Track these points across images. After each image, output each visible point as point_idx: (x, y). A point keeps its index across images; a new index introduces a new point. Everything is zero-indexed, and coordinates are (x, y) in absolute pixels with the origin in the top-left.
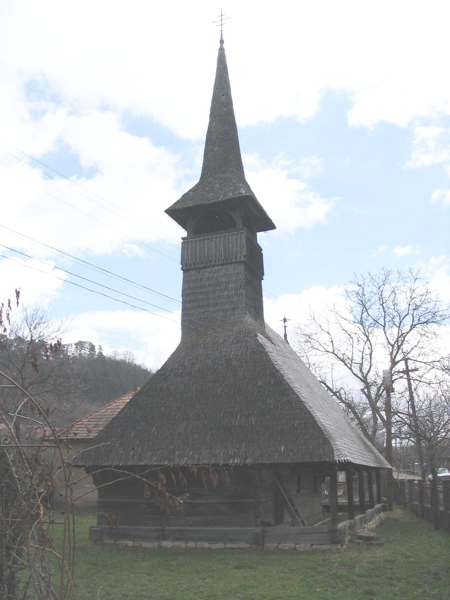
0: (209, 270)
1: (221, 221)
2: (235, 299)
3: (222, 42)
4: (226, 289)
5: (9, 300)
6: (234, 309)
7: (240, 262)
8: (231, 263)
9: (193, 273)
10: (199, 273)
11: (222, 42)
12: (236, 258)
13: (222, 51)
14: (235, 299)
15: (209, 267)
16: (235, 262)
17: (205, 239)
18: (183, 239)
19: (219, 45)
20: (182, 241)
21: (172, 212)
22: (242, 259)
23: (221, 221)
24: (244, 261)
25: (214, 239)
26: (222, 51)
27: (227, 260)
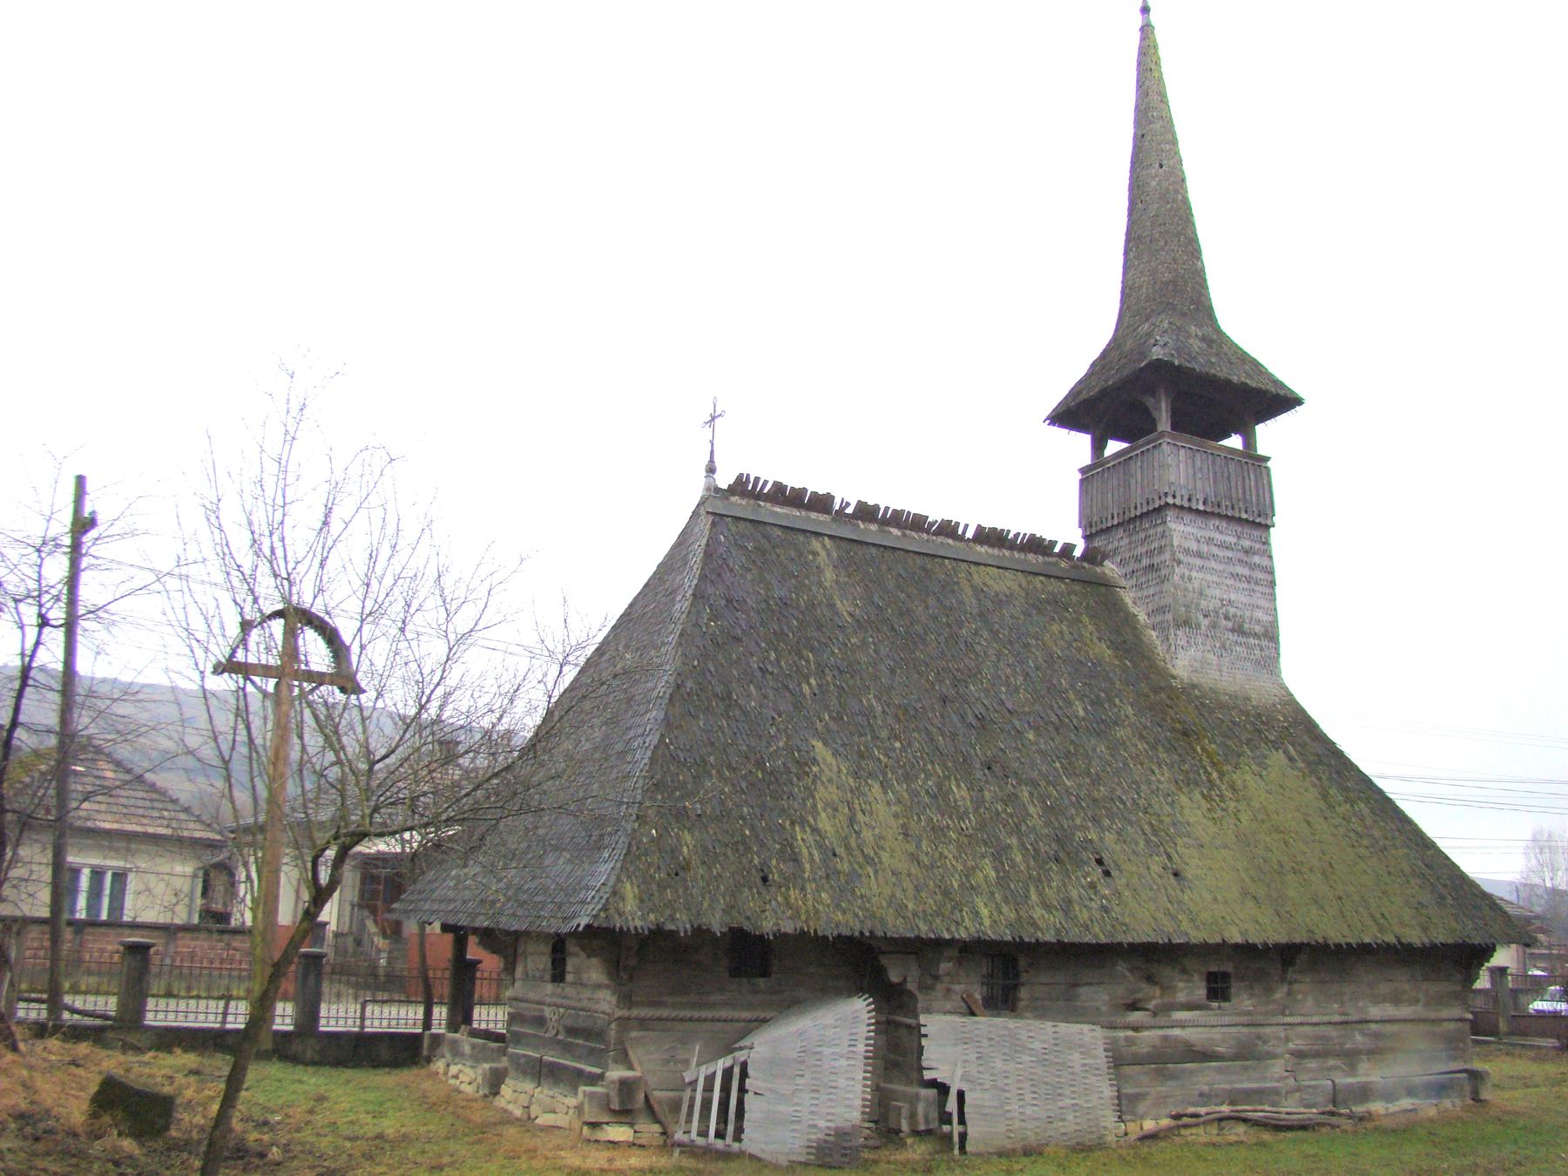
3: (1145, 10)
5: (81, 481)
11: (1145, 10)
13: (1146, 30)
19: (1138, 21)
21: (1068, 416)
23: (1174, 396)
26: (1146, 30)
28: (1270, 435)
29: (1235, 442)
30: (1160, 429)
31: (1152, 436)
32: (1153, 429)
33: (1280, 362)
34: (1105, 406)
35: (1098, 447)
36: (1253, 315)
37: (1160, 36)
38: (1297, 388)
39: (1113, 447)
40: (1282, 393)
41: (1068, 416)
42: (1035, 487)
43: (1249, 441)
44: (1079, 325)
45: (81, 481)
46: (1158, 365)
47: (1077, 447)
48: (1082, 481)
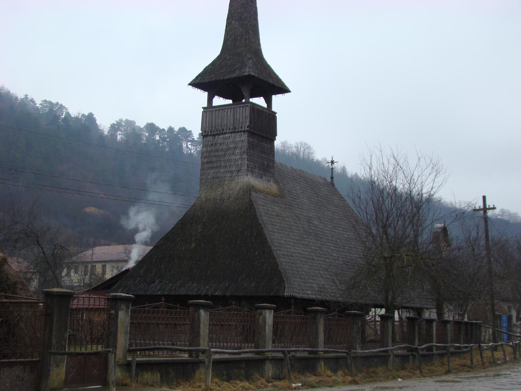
0: (222, 136)
1: (240, 77)
2: (240, 162)
4: (233, 154)
5: (484, 198)
6: (239, 171)
7: (244, 131)
8: (238, 132)
9: (210, 138)
10: (215, 138)
12: (241, 128)
14: (240, 162)
15: (222, 134)
16: (241, 132)
18: (204, 108)
20: (203, 110)
22: (246, 129)
24: (247, 131)
25: (226, 110)
27: (235, 129)
29: (260, 101)
35: (210, 100)
38: (290, 89)
39: (218, 101)
43: (269, 101)
44: (209, 48)
45: (484, 198)
47: (201, 97)
48: (203, 112)
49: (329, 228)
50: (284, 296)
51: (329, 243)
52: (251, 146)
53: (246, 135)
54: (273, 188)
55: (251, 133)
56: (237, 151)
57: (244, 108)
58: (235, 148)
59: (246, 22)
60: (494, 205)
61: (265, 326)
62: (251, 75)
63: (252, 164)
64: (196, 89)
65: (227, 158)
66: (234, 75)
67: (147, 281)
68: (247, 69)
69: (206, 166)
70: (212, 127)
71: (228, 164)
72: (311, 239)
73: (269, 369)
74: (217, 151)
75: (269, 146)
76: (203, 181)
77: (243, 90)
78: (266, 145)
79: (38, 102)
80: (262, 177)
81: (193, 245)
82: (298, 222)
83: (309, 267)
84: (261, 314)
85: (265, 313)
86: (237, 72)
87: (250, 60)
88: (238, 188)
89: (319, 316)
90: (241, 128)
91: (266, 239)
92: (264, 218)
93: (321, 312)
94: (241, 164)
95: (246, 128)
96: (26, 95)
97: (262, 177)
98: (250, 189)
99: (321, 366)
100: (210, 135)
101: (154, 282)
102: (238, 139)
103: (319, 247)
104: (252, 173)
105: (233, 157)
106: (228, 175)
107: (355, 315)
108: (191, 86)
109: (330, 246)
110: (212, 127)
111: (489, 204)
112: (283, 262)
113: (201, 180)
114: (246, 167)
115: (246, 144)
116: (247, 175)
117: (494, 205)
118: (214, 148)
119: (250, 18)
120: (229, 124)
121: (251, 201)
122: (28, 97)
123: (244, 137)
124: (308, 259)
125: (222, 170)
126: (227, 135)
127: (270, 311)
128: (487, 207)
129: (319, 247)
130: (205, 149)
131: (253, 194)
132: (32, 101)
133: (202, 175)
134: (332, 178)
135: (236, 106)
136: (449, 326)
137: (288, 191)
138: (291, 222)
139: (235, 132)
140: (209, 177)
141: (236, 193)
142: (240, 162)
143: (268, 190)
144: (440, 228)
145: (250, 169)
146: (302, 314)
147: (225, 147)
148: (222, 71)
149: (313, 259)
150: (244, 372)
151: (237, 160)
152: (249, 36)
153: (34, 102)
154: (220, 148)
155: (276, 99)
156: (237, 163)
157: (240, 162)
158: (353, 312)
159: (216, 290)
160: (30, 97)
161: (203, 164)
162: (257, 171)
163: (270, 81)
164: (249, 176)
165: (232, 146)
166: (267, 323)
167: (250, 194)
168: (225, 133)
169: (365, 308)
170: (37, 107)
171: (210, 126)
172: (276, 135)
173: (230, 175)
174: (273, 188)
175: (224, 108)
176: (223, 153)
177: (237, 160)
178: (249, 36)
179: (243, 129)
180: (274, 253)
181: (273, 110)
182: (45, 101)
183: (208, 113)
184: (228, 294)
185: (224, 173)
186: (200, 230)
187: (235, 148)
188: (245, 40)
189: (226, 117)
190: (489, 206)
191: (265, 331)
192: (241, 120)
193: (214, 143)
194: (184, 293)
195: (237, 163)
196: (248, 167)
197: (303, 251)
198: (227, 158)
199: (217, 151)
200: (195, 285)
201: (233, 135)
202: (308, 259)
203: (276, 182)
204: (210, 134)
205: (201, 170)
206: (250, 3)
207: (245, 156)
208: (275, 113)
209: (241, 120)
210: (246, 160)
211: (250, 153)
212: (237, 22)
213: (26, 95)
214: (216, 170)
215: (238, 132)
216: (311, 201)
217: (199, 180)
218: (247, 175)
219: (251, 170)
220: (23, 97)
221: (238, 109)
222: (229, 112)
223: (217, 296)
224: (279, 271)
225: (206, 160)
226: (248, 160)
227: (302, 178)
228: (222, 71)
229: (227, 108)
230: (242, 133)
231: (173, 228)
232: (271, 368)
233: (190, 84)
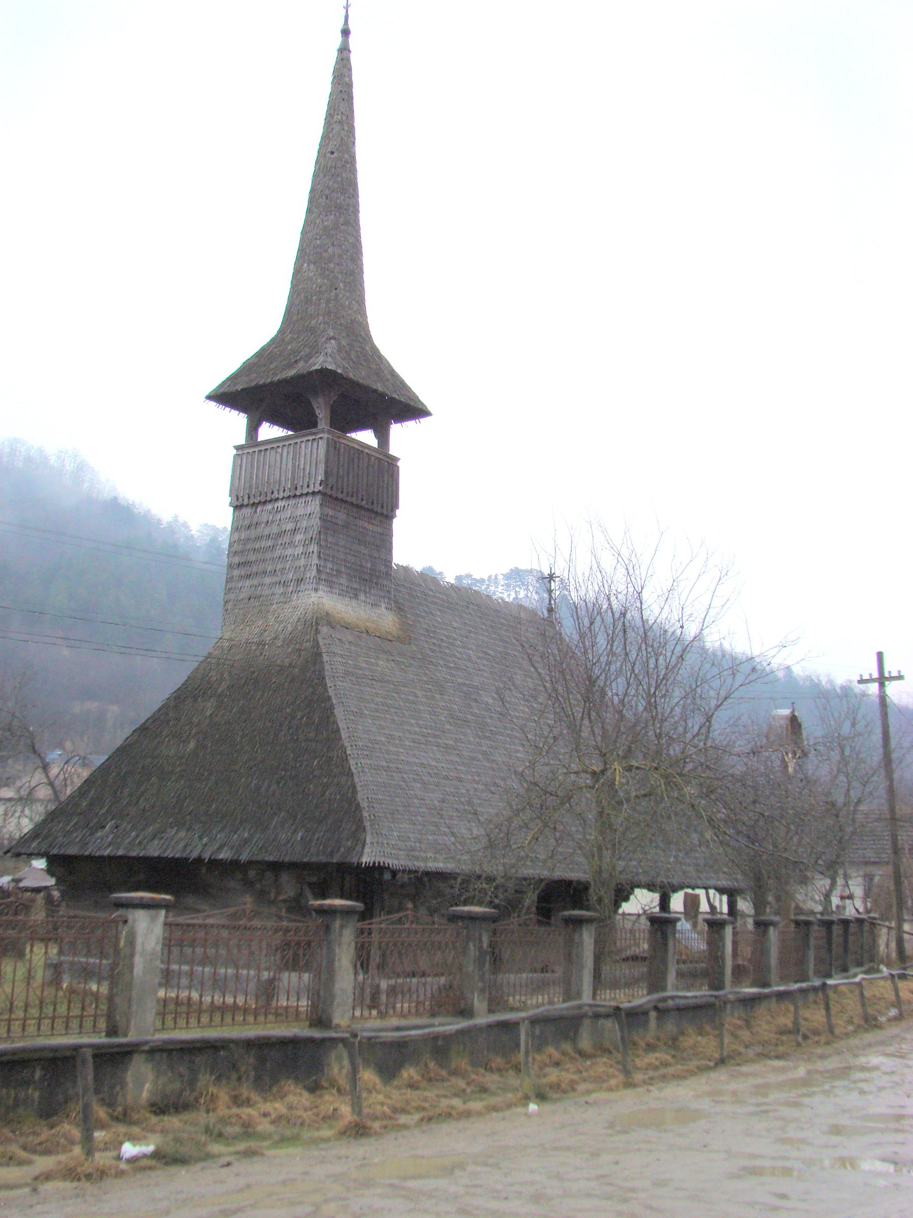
0: (269, 507)
1: (321, 395)
2: (302, 562)
3: (346, 33)
4: (291, 544)
5: (880, 656)
6: (300, 581)
7: (314, 493)
8: (301, 495)
9: (247, 511)
10: (256, 512)
11: (346, 33)
12: (308, 486)
13: (344, 51)
14: (302, 562)
15: (270, 501)
16: (307, 494)
17: (266, 450)
18: (238, 448)
19: (338, 39)
20: (235, 452)
21: (225, 397)
22: (318, 488)
23: (321, 395)
24: (319, 492)
25: (280, 450)
26: (344, 51)
27: (296, 488)
28: (403, 437)
29: (367, 437)
30: (320, 427)
31: (314, 430)
32: (315, 425)
33: (417, 378)
34: (261, 393)
35: (253, 430)
36: (400, 331)
37: (355, 60)
38: (430, 408)
39: (268, 432)
40: (359, 375)
41: (225, 397)
42: (546, 614)
43: (383, 436)
44: (251, 319)
45: (880, 656)
46: (325, 374)
47: (235, 423)
48: (236, 456)
49: (523, 712)
50: (359, 864)
51: (514, 744)
52: (327, 524)
53: (318, 502)
54: (386, 620)
55: (330, 496)
56: (299, 537)
57: (315, 444)
58: (294, 531)
59: (332, 265)
60: (899, 672)
61: (132, 955)
62: (327, 369)
63: (329, 565)
64: (228, 409)
65: (277, 553)
66: (292, 373)
67: (91, 825)
68: (321, 358)
69: (236, 573)
70: (251, 488)
71: (279, 566)
72: (465, 734)
73: (142, 1081)
74: (259, 538)
75: (379, 530)
76: (229, 607)
77: (315, 405)
78: (370, 527)
79: (195, 529)
80: (356, 597)
81: (192, 745)
82: (438, 696)
83: (426, 798)
84: (126, 922)
85: (134, 921)
86: (301, 364)
87: (333, 341)
88: (295, 618)
89: (337, 923)
90: (308, 486)
91: (338, 730)
92: (337, 686)
93: (347, 913)
94: (305, 566)
95: (317, 485)
96: (176, 516)
97: (356, 597)
98: (319, 621)
99: (338, 1067)
100: (247, 505)
101: (104, 827)
102: (300, 511)
103: (485, 754)
104: (331, 585)
105: (289, 551)
106: (279, 590)
107: (472, 918)
108: (213, 404)
109: (518, 751)
110: (251, 488)
111: (890, 668)
112: (368, 784)
113: (226, 602)
114: (314, 573)
115: (316, 521)
116: (316, 590)
117: (899, 672)
118: (253, 533)
119: (339, 256)
120: (283, 478)
121: (317, 645)
122: (179, 519)
123: (314, 505)
124: (446, 778)
125: (268, 580)
126: (280, 504)
127: (152, 912)
128: (887, 675)
129: (485, 754)
130: (236, 536)
131: (324, 630)
132: (185, 525)
133: (229, 591)
134: (550, 610)
135: (299, 441)
136: (835, 927)
137: (428, 631)
138: (417, 697)
139: (295, 496)
140: (242, 596)
141: (290, 628)
142: (303, 560)
143: (369, 624)
144: (782, 717)
145: (323, 577)
146: (280, 918)
147: (275, 529)
148: (272, 366)
149: (460, 780)
150: (37, 1094)
151: (298, 558)
152: (337, 295)
153: (188, 527)
154: (266, 532)
155: (397, 431)
156: (297, 563)
157: (303, 560)
158: (466, 908)
159: (220, 848)
160: (181, 520)
161: (230, 566)
162: (344, 581)
163: (380, 387)
164: (320, 593)
165: (290, 526)
166: (138, 948)
167: (317, 632)
168: (277, 499)
169: (622, 894)
170: (192, 536)
171: (247, 485)
172: (397, 507)
173: (282, 590)
174: (386, 620)
175: (275, 445)
176: (270, 543)
177: (298, 558)
178: (337, 295)
179: (311, 490)
180: (352, 762)
181: (390, 453)
182: (206, 525)
183: (245, 457)
184: (244, 857)
185: (272, 585)
186: (208, 713)
187: (294, 531)
188: (328, 302)
189: (278, 464)
190: (890, 672)
191: (132, 971)
192: (308, 471)
193: (254, 523)
194: (156, 854)
195: (297, 563)
196: (319, 571)
197: (437, 760)
198: (277, 553)
199: (259, 538)
200: (182, 834)
201: (292, 502)
202: (446, 778)
203: (399, 608)
204: (246, 502)
205: (227, 582)
206: (343, 227)
207: (314, 548)
208: (396, 459)
209: (308, 471)
210: (315, 555)
211: (326, 540)
212: (312, 266)
213: (176, 516)
214: (255, 582)
215: (301, 495)
216: (486, 653)
217: (223, 603)
218: (316, 590)
219: (327, 579)
220: (171, 519)
221: (303, 445)
222: (285, 454)
223: (222, 860)
224: (358, 805)
225: (236, 560)
226: (319, 557)
227: (471, 606)
228: (272, 366)
229: (281, 444)
230: (309, 498)
231: (159, 710)
232: (151, 1076)
233: (210, 397)
